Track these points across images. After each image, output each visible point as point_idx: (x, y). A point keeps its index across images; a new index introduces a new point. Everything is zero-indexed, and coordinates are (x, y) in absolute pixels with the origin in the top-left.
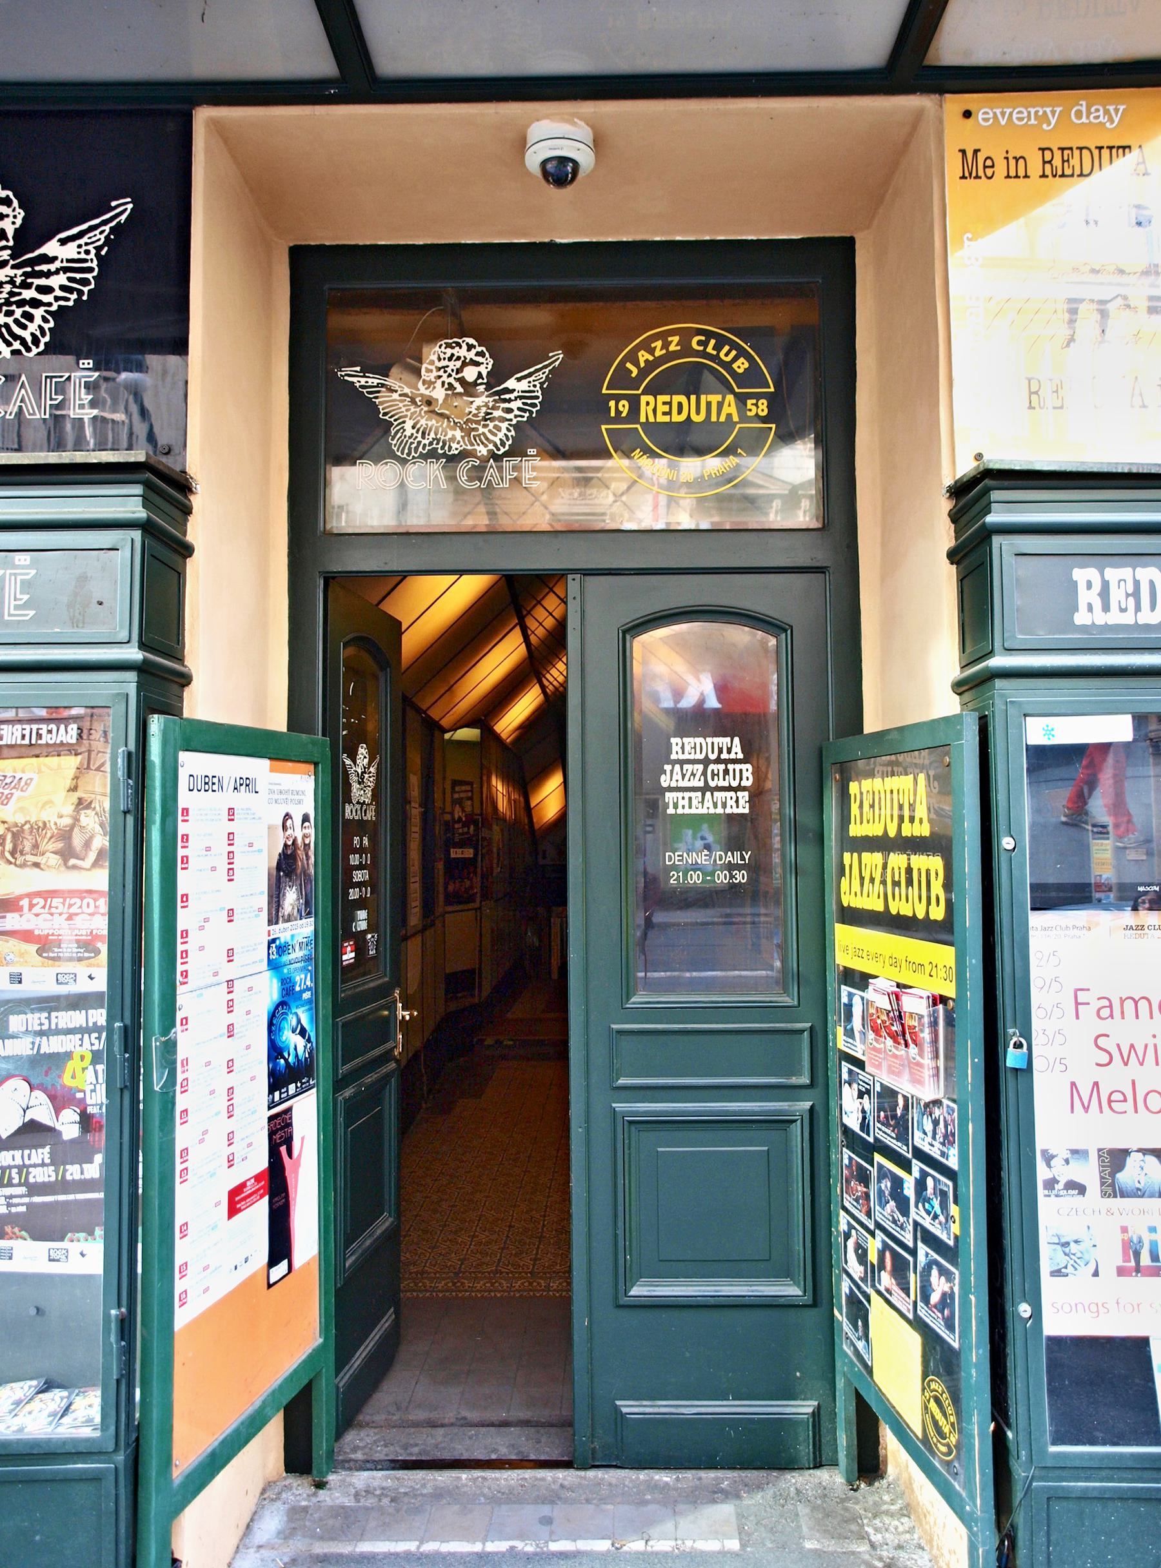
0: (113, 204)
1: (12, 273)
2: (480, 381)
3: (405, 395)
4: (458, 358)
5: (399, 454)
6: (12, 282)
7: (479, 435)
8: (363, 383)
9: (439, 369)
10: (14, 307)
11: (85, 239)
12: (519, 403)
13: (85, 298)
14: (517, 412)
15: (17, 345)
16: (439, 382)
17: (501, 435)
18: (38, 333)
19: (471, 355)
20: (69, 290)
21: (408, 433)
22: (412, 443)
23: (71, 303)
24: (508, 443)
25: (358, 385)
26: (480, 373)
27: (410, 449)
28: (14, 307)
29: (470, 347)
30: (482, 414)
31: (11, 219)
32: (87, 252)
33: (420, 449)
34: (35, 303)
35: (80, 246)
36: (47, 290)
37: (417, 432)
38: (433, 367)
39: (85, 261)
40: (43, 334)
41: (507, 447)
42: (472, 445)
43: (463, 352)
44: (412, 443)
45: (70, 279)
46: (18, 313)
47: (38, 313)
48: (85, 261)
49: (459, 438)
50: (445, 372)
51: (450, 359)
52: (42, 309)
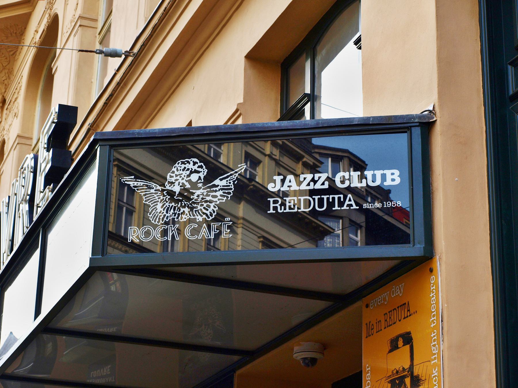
0: (239, 166)
1: (203, 191)
2: (200, 181)
3: (158, 190)
4: (188, 169)
5: (153, 222)
6: (203, 194)
7: (198, 211)
8: (135, 185)
9: (176, 176)
10: (203, 203)
11: (229, 179)
12: (221, 192)
13: (229, 199)
14: (219, 197)
15: (204, 216)
16: (177, 182)
17: (210, 210)
18: (212, 212)
19: (195, 167)
20: (224, 196)
21: (158, 211)
22: (160, 216)
23: (224, 201)
24: (214, 214)
25: (132, 186)
26: (200, 177)
27: (159, 219)
28: (203, 203)
29: (195, 163)
30: (200, 199)
31: (203, 173)
32: (230, 183)
33: (165, 219)
34: (211, 202)
35: (227, 181)
36: (215, 197)
37: (164, 210)
38: (174, 175)
39: (229, 186)
40: (214, 212)
41: (213, 217)
42: (194, 216)
43: (190, 166)
44: (160, 216)
45: (224, 193)
46: (205, 205)
47: (212, 205)
48: (229, 186)
49: (186, 212)
50: (180, 177)
51: (183, 170)
52: (214, 203)
